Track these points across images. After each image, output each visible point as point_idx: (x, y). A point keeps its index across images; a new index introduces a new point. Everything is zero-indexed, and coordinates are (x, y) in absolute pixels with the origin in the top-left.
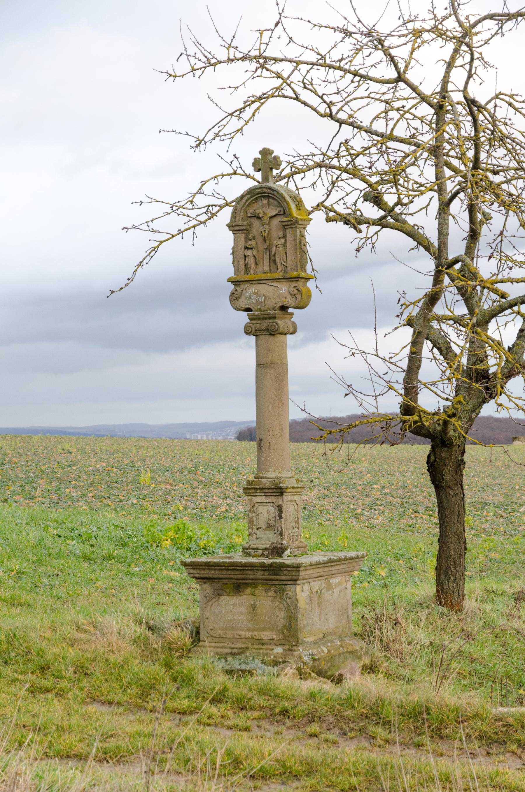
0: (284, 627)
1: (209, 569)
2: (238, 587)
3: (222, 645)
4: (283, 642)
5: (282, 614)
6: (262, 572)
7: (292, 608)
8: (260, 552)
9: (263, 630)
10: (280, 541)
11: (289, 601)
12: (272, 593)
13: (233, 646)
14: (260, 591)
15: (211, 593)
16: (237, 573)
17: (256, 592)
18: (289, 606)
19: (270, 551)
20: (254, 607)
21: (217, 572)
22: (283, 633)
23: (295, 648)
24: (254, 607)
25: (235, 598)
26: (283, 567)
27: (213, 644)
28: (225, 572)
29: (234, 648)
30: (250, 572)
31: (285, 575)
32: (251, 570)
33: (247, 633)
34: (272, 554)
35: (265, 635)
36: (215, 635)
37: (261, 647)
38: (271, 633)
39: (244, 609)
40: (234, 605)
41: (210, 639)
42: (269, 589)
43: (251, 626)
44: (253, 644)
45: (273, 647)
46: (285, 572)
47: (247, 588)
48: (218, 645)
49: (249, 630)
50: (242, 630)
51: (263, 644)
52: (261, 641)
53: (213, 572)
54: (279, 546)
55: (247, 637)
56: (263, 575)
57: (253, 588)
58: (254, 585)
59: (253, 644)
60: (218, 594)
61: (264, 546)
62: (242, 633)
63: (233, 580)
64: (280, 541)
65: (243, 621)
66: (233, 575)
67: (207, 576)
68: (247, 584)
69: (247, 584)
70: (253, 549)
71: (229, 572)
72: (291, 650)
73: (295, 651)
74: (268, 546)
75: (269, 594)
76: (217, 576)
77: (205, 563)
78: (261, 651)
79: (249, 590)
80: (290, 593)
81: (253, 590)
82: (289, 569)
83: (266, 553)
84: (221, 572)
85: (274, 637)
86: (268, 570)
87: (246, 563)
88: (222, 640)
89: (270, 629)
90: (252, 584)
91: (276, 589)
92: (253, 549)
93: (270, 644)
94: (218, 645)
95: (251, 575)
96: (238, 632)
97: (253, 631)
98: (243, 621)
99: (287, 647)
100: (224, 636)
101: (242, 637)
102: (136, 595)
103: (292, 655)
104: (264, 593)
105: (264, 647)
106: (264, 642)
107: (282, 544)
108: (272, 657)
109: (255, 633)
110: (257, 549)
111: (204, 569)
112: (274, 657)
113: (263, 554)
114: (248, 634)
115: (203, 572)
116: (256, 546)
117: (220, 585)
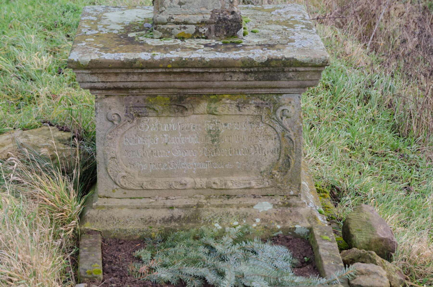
0: (273, 165)
1: (128, 74)
2: (180, 103)
3: (144, 202)
4: (270, 191)
5: (271, 145)
6: (241, 76)
7: (292, 133)
8: (192, 29)
9: (232, 172)
10: (228, 7)
11: (285, 122)
12: (251, 109)
13: (169, 203)
14: (226, 107)
15: (122, 115)
16: (188, 78)
17: (219, 109)
18: (285, 129)
19: (212, 27)
20: (214, 136)
21: (144, 78)
22: (272, 176)
23: (294, 200)
24: (214, 136)
25: (172, 120)
26: (291, 66)
27: (127, 202)
28: (162, 77)
29: (172, 208)
30: (216, 77)
31: (289, 79)
32: (219, 73)
33: (198, 180)
34: (216, 31)
35: (235, 182)
36: (131, 186)
37: (226, 202)
38: (246, 178)
39: (193, 140)
40: (171, 133)
41: (119, 193)
42: (246, 103)
43: (206, 168)
44: (208, 198)
45: (251, 201)
46: (291, 74)
47: (199, 103)
48: (137, 202)
49: (200, 174)
50: (187, 175)
51: (229, 197)
52: (226, 193)
53: (136, 78)
54: (231, 17)
55: (198, 186)
56: (245, 80)
57: (211, 101)
58: (215, 97)
59: (208, 198)
60: (136, 114)
61: (199, 18)
62: (188, 180)
63: (171, 90)
64: (228, 7)
65: (189, 160)
66: (178, 82)
67: (121, 85)
68: (200, 96)
69: (200, 96)
70: (177, 23)
71: (172, 77)
72: (289, 205)
73: (296, 206)
74: (208, 17)
75: (245, 111)
76: (143, 84)
77: (122, 63)
78: (232, 211)
79: (203, 106)
80: (290, 108)
81: (213, 105)
82: (302, 69)
83: (204, 30)
84: (153, 78)
85: (253, 184)
86: (255, 72)
87: (212, 61)
88: (146, 194)
89: (246, 171)
90: (209, 95)
91: (259, 101)
92: (177, 23)
93: (244, 196)
94: (137, 202)
95: (217, 80)
96: (178, 179)
97: (209, 175)
98: (189, 160)
99: (279, 200)
100: (149, 187)
101: (188, 186)
102: (364, 192)
103: (297, 214)
104: (234, 110)
105: (234, 201)
106: (232, 193)
107: (233, 13)
108: (258, 220)
109: (216, 179)
110: (186, 23)
111: (117, 74)
112: (262, 220)
113: (197, 31)
114: (201, 182)
115: (113, 78)
116: (182, 18)
117: (141, 98)
